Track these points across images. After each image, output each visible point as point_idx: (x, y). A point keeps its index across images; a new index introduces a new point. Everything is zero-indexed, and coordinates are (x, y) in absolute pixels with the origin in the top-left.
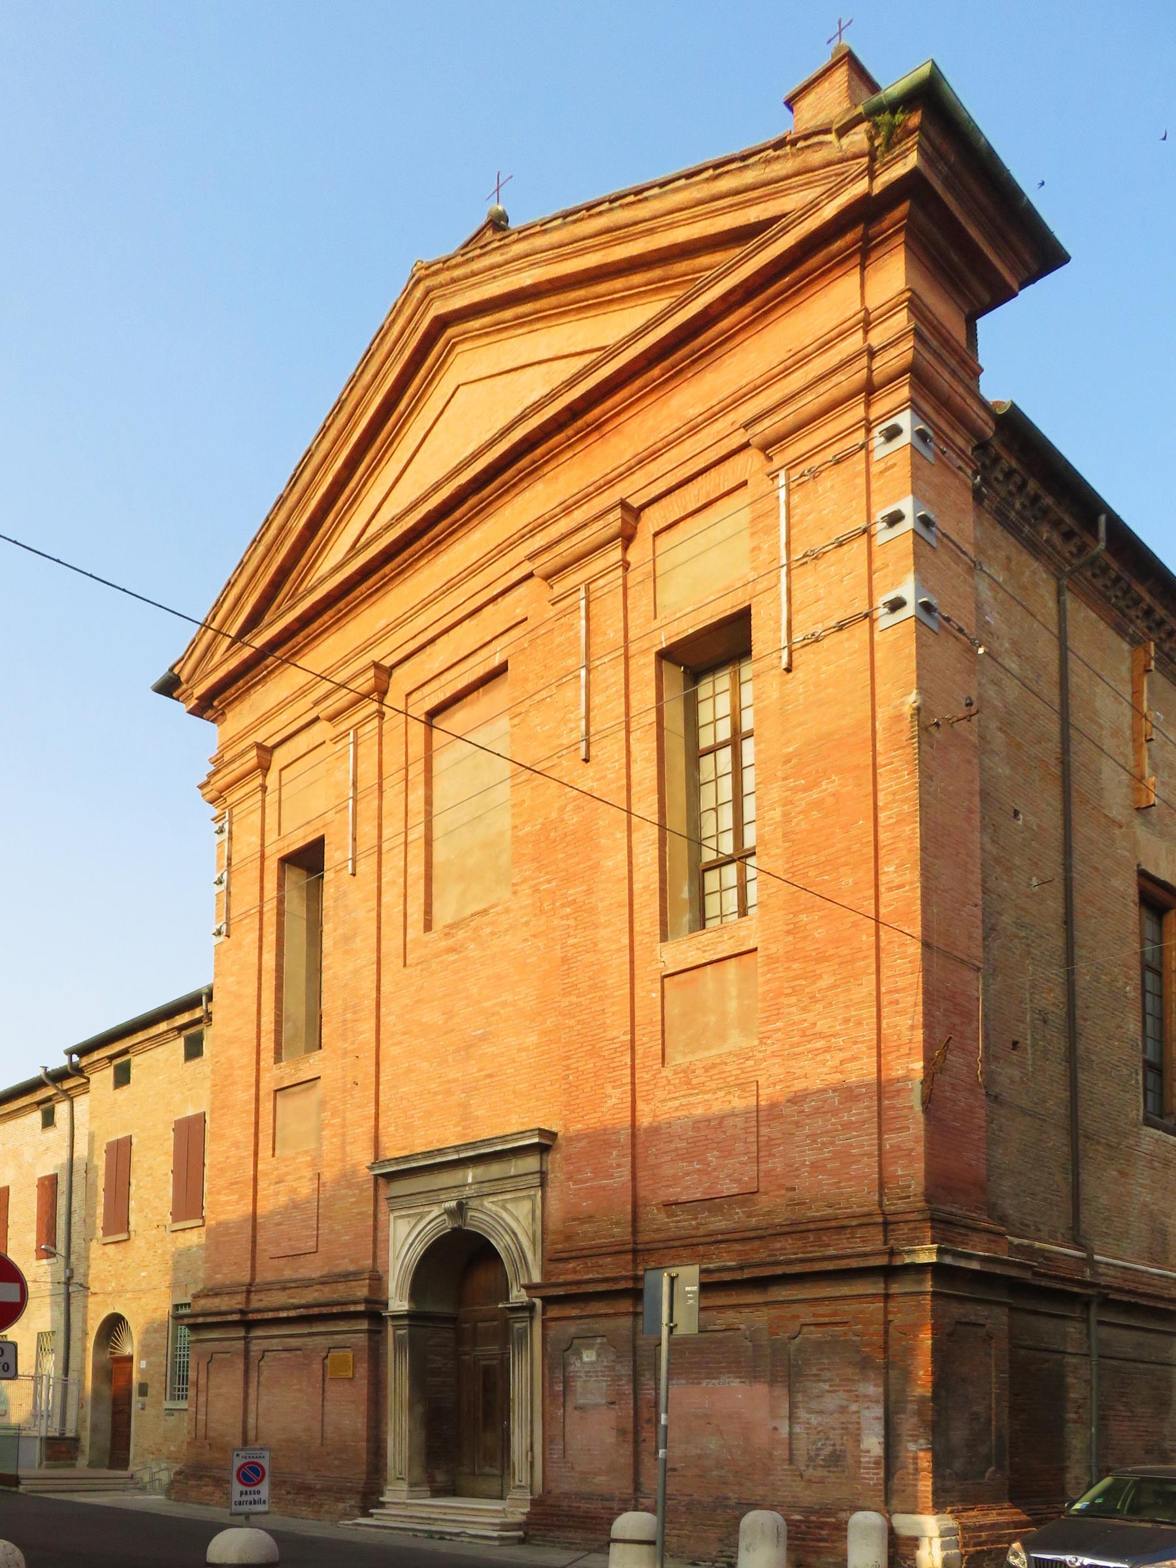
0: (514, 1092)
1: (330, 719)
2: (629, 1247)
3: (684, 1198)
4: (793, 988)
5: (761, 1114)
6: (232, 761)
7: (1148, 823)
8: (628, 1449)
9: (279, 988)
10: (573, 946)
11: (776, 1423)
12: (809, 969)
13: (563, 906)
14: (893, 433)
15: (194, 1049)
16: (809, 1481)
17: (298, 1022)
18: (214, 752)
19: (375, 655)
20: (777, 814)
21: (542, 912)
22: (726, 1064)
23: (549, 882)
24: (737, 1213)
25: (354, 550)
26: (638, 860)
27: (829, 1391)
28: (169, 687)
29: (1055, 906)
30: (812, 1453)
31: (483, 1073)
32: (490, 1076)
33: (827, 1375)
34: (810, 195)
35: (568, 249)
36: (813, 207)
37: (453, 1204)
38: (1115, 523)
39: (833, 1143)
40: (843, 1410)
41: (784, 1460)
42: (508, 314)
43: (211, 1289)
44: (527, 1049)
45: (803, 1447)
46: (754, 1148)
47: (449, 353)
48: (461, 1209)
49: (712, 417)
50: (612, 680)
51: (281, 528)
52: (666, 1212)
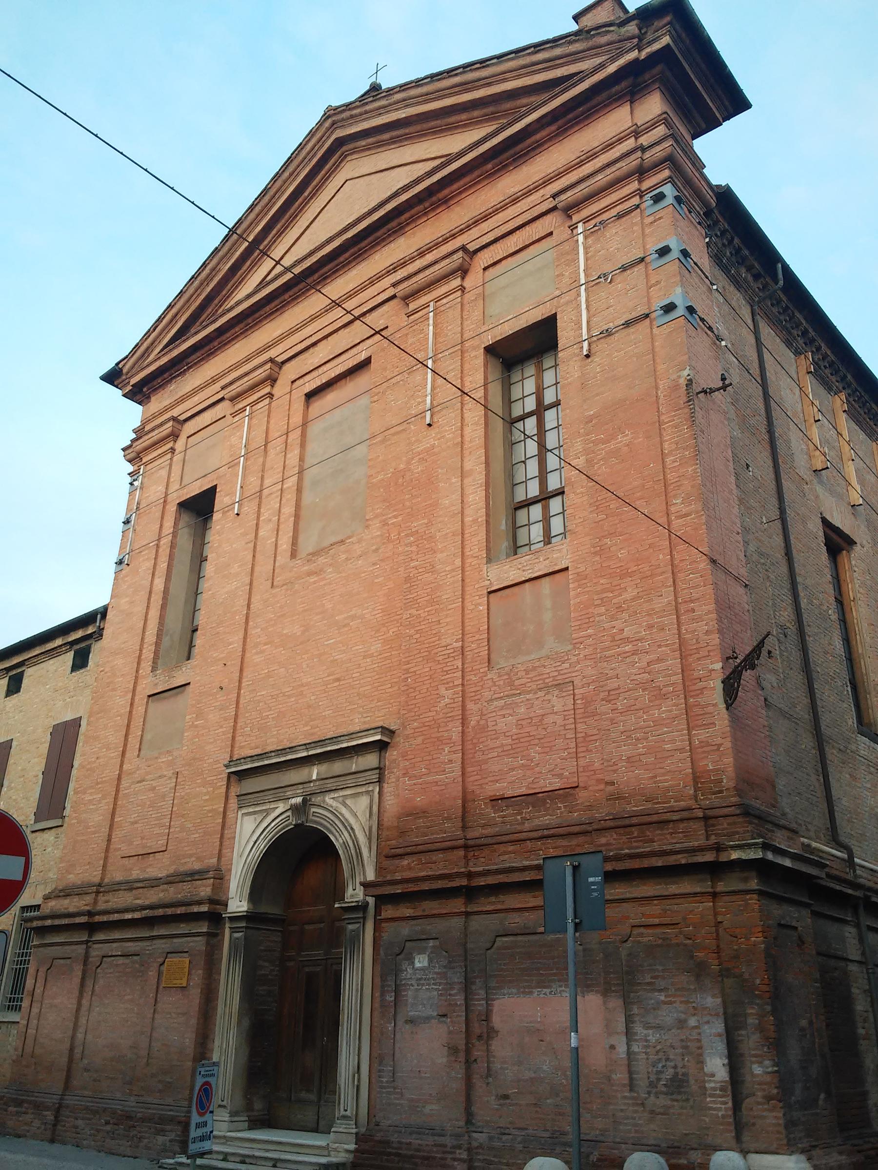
0: (358, 694)
1: (232, 399)
2: (461, 842)
3: (509, 793)
4: (602, 599)
5: (577, 712)
6: (153, 430)
7: (821, 482)
8: (459, 1072)
9: (163, 607)
10: (415, 567)
11: (613, 1041)
12: (615, 583)
13: (407, 536)
15: (81, 661)
16: (652, 1112)
17: (180, 637)
18: (137, 423)
22: (545, 667)
23: (395, 517)
24: (560, 808)
27: (665, 1003)
28: (112, 377)
29: (779, 540)
30: (653, 1077)
32: (338, 680)
33: (662, 984)
34: (598, 61)
35: (432, 96)
37: (299, 800)
38: (786, 269)
40: (681, 1024)
41: (624, 1085)
42: (386, 136)
43: (61, 891)
44: (371, 656)
45: (642, 1067)
46: (573, 745)
47: (342, 161)
49: (528, 192)
50: (451, 368)
51: (213, 269)
52: (493, 807)
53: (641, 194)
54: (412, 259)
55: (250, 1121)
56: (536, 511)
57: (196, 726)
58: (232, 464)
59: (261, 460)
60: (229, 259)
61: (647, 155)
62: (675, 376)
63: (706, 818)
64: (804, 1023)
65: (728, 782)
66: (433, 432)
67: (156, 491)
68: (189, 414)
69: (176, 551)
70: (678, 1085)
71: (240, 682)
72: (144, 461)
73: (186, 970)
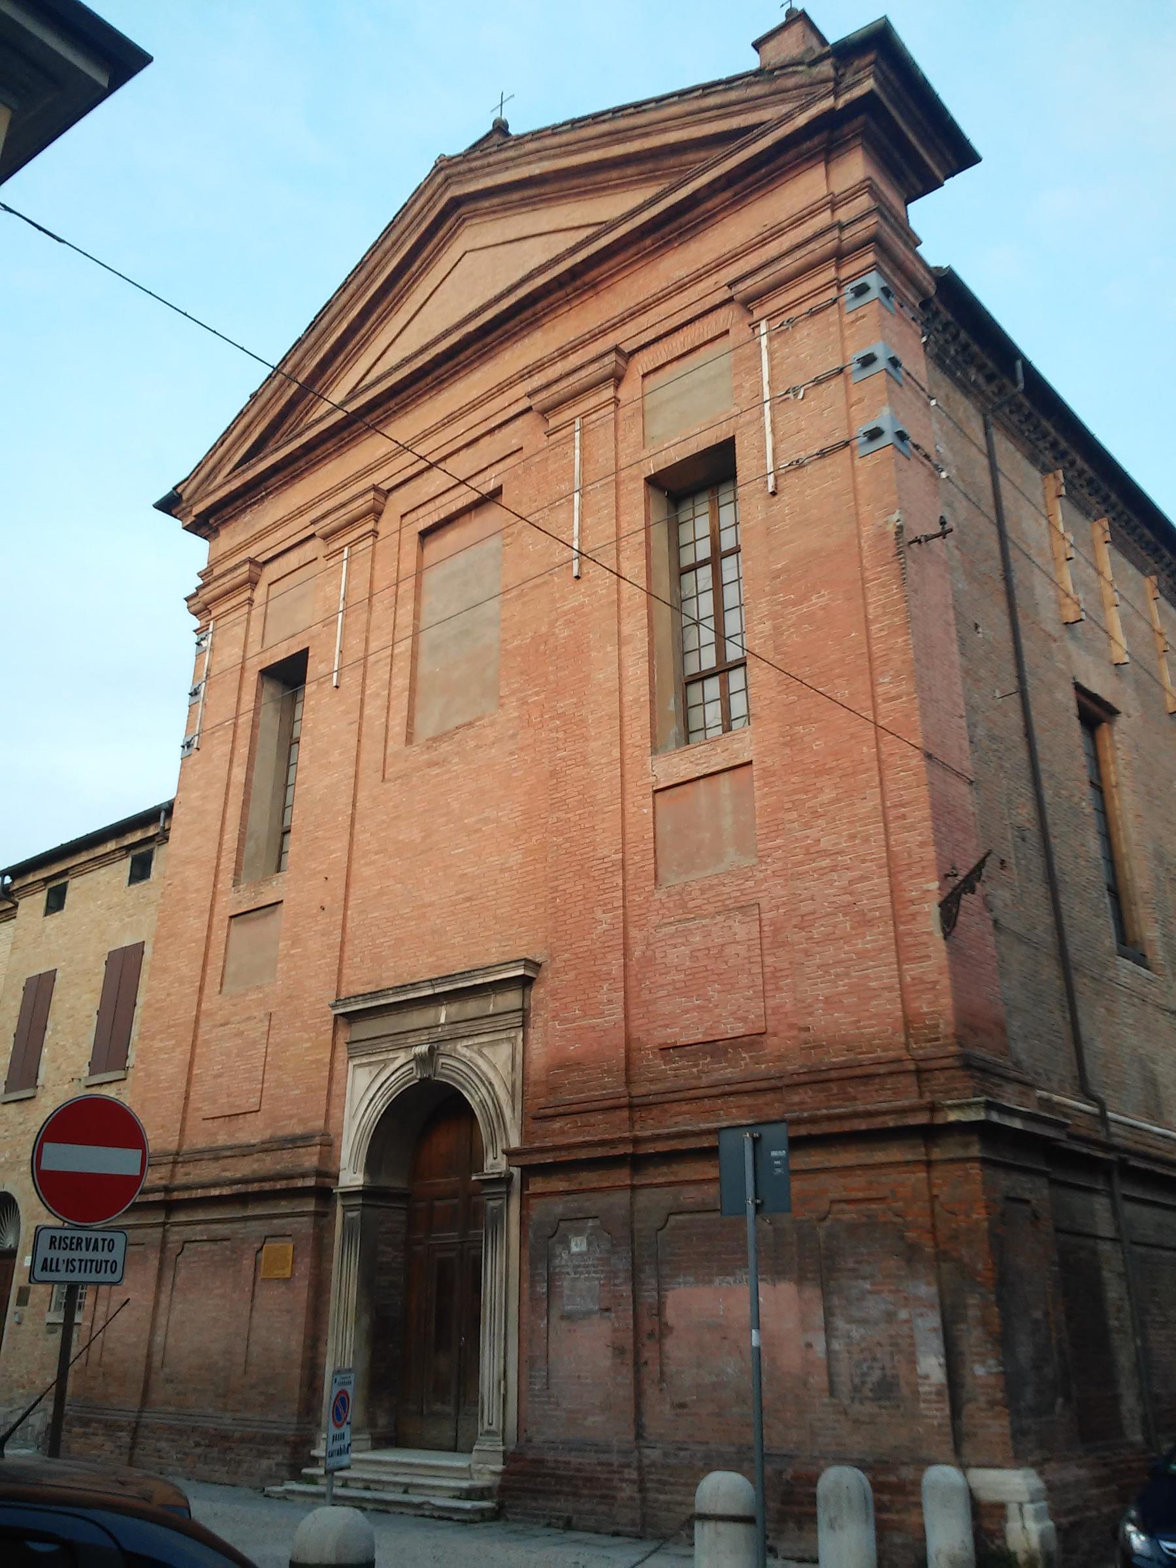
0: (495, 917)
1: (325, 537)
2: (624, 1101)
3: (683, 1040)
6: (223, 575)
7: (1074, 638)
9: (246, 803)
10: (562, 759)
12: (808, 783)
13: (552, 718)
14: (862, 290)
15: (141, 870)
16: (856, 1421)
18: (203, 565)
19: (374, 479)
20: (766, 627)
21: (529, 724)
23: (537, 694)
25: (353, 394)
26: (630, 672)
27: (870, 1292)
28: (169, 505)
29: (1016, 718)
30: (857, 1380)
31: (461, 896)
32: (469, 899)
33: (866, 1269)
34: (784, 109)
36: (789, 117)
37: (424, 1049)
39: (847, 975)
40: (890, 1317)
42: (516, 196)
44: (510, 869)
45: (844, 1369)
46: (760, 981)
47: (459, 226)
48: (422, 1061)
49: (698, 278)
52: (663, 1058)
53: (839, 284)
54: (552, 361)
55: (373, 1439)
56: (712, 687)
57: (293, 955)
58: (328, 622)
59: (365, 616)
60: (316, 353)
61: (846, 234)
62: (880, 522)
63: (918, 1072)
64: (1038, 1314)
65: (946, 1027)
66: (582, 586)
67: (230, 654)
68: (270, 554)
69: (259, 731)
70: (886, 1389)
71: (346, 899)
72: (214, 614)
73: (290, 1258)
